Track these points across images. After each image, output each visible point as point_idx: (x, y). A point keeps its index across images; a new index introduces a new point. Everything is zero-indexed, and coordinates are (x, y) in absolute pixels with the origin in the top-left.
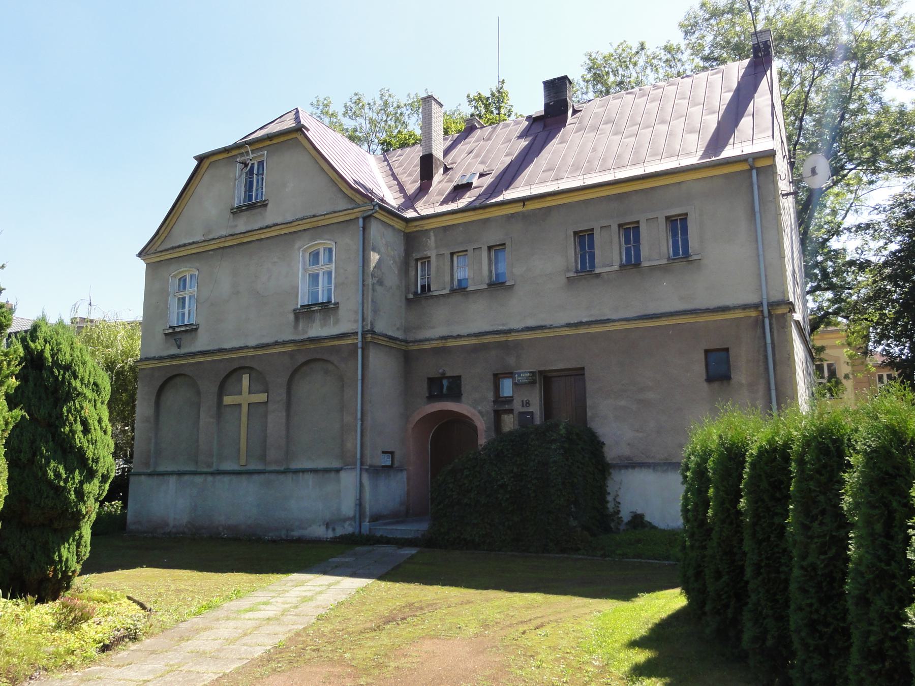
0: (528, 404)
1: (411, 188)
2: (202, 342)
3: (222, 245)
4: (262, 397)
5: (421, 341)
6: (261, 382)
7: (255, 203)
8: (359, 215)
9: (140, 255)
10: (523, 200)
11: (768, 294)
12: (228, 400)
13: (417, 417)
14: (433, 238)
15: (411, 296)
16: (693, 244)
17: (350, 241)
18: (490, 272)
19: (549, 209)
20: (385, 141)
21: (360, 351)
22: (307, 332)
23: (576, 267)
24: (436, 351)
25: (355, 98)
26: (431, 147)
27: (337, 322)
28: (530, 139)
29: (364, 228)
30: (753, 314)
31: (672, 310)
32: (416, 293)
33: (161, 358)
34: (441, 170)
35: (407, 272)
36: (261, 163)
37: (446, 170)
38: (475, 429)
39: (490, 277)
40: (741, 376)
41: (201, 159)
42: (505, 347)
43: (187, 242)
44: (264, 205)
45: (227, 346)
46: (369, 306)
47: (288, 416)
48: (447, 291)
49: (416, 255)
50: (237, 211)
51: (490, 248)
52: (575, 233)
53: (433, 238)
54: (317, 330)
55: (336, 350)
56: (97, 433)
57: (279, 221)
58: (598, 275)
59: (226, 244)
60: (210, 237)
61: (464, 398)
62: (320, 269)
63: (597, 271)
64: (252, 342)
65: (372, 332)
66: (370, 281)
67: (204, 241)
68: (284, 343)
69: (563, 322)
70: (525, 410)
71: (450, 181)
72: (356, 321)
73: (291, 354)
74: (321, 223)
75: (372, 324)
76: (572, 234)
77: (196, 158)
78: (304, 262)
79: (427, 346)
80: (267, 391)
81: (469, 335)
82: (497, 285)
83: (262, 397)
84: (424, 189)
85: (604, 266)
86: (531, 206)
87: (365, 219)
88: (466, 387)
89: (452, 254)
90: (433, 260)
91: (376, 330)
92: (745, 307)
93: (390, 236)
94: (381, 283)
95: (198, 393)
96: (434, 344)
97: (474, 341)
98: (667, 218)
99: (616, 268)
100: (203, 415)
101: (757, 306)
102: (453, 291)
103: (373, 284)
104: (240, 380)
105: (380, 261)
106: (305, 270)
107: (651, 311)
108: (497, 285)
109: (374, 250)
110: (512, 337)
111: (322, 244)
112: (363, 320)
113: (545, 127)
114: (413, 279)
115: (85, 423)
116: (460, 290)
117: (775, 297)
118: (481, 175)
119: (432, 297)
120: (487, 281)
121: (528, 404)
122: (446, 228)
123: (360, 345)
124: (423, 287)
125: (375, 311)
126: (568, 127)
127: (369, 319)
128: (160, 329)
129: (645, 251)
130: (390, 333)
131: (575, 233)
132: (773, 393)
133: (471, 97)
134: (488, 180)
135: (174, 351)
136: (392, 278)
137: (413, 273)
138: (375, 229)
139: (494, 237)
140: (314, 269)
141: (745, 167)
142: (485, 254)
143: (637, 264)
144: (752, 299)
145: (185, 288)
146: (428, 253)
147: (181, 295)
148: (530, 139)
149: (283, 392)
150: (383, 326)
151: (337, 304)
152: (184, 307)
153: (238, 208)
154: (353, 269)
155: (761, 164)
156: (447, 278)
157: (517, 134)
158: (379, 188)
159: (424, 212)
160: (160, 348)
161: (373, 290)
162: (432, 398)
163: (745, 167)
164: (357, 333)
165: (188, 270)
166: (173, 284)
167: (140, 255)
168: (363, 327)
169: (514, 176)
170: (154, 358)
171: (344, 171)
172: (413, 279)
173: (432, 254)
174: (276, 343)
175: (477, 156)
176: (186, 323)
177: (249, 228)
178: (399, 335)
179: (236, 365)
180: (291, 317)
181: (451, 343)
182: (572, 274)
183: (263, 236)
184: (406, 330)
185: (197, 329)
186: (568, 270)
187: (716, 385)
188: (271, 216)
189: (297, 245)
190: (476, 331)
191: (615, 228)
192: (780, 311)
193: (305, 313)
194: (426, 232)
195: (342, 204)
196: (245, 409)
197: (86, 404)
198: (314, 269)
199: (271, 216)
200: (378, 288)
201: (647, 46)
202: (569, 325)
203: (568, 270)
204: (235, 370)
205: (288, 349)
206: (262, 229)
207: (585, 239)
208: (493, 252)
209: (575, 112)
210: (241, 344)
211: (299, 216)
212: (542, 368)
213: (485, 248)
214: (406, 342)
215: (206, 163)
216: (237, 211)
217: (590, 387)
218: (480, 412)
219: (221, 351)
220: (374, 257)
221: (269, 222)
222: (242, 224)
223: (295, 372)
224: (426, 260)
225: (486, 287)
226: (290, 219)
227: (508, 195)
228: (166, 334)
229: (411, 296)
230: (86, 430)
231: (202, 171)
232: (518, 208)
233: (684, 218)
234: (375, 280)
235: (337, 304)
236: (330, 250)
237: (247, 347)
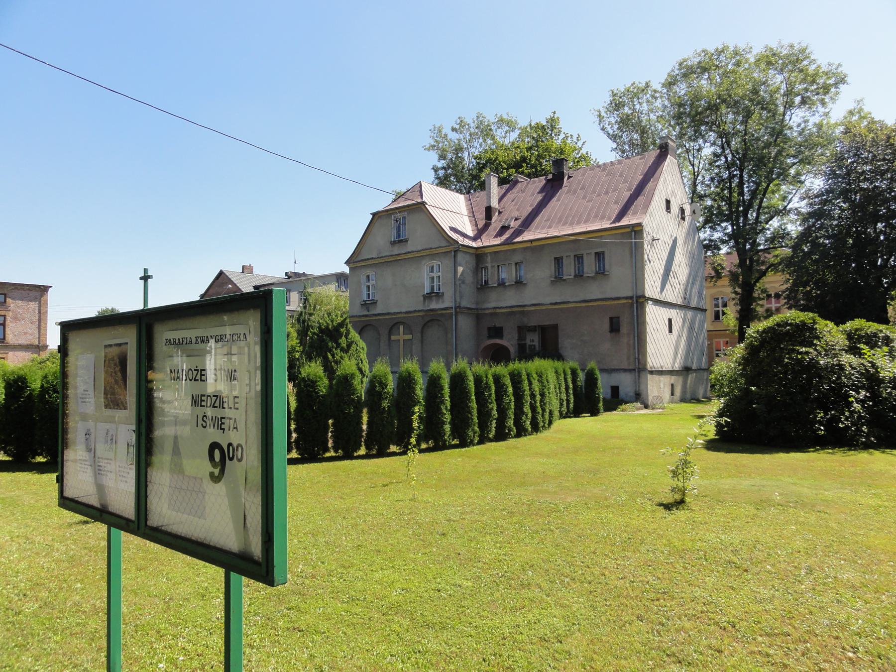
0: (533, 341)
1: (481, 224)
2: (379, 309)
3: (387, 260)
4: (410, 337)
5: (484, 309)
6: (409, 329)
7: (402, 240)
8: (452, 249)
9: (346, 263)
10: (531, 241)
11: (636, 292)
12: (393, 338)
13: (483, 346)
14: (489, 257)
15: (479, 287)
16: (607, 267)
17: (448, 262)
18: (516, 275)
19: (543, 245)
20: (477, 157)
21: (454, 317)
22: (429, 306)
23: (555, 275)
24: (492, 314)
25: (458, 122)
26: (490, 203)
27: (443, 302)
28: (544, 194)
29: (455, 256)
30: (630, 301)
31: (595, 298)
32: (481, 285)
33: (360, 316)
34: (497, 214)
35: (477, 274)
36: (404, 218)
37: (500, 213)
38: (509, 352)
39: (516, 277)
40: (624, 330)
41: (374, 215)
42: (523, 313)
43: (369, 257)
44: (406, 241)
45: (392, 311)
46: (458, 294)
47: (422, 337)
48: (496, 285)
49: (481, 266)
50: (393, 243)
51: (516, 264)
52: (555, 258)
53: (489, 257)
54: (434, 305)
55: (442, 315)
56: (365, 363)
57: (414, 250)
58: (565, 280)
59: (389, 260)
60: (381, 256)
61: (504, 337)
62: (435, 275)
63: (564, 278)
64: (404, 310)
65: (459, 307)
66: (458, 283)
67: (378, 258)
68: (419, 311)
69: (548, 302)
70: (532, 344)
71: (500, 221)
72: (452, 302)
73: (423, 317)
74: (434, 253)
75: (459, 303)
76: (553, 259)
77: (371, 214)
78: (427, 272)
79: (487, 312)
80: (411, 334)
81: (507, 307)
82: (519, 283)
83: (410, 337)
84: (487, 226)
85: (567, 276)
86: (534, 244)
87: (455, 251)
88: (505, 333)
89: (498, 266)
90: (490, 268)
91: (462, 306)
92: (627, 298)
93: (467, 257)
94: (463, 282)
95: (379, 334)
96: (490, 311)
97: (508, 310)
98: (596, 253)
99: (572, 277)
100: (382, 345)
101: (631, 298)
102: (499, 285)
103: (460, 284)
104: (399, 329)
105: (463, 271)
106: (427, 275)
107: (588, 298)
108: (519, 283)
109: (460, 266)
110: (526, 309)
111: (435, 263)
112: (455, 301)
113: (552, 187)
114: (480, 278)
115: (361, 360)
116: (502, 284)
117: (640, 294)
118: (516, 219)
119: (489, 287)
120: (514, 281)
121: (533, 341)
122: (496, 253)
123: (454, 313)
124: (485, 281)
125: (461, 297)
126: (563, 188)
127: (458, 300)
128: (358, 302)
129: (586, 269)
130: (469, 306)
131: (555, 258)
132: (636, 338)
133: (532, 125)
134: (519, 222)
135: (366, 313)
136: (469, 279)
137: (480, 275)
138: (460, 256)
139: (517, 258)
140: (432, 275)
141: (628, 230)
142: (513, 267)
143: (582, 276)
144: (629, 294)
145: (369, 280)
146: (487, 265)
147: (368, 284)
148: (544, 194)
149: (419, 335)
150: (464, 304)
151: (443, 293)
152: (369, 291)
153: (394, 241)
154: (450, 275)
155: (636, 229)
156: (496, 278)
157: (538, 191)
158: (463, 225)
159: (486, 244)
160: (358, 311)
161: (460, 286)
162: (490, 337)
163: (628, 230)
164: (452, 308)
165: (370, 272)
166: (364, 278)
167: (346, 263)
168: (455, 305)
169: (536, 213)
170: (356, 316)
171: (444, 223)
172: (480, 278)
173: (489, 265)
174: (415, 311)
175: (515, 205)
176: (371, 299)
177: (399, 252)
178: (473, 306)
179: (396, 321)
180: (422, 299)
181: (498, 311)
182: (553, 279)
183: (406, 257)
184: (477, 303)
185: (376, 302)
186: (551, 277)
187: (613, 334)
188: (410, 247)
189: (424, 262)
190: (510, 305)
191: (572, 257)
192: (641, 300)
193: (428, 297)
194: (486, 254)
195: (444, 243)
196: (402, 342)
197: (361, 354)
198: (432, 275)
199: (410, 247)
200: (462, 285)
201: (651, 84)
202: (551, 304)
203: (551, 277)
204: (398, 323)
205: (421, 314)
206: (406, 253)
207: (558, 261)
208: (518, 266)
209: (569, 177)
210: (397, 311)
211: (424, 248)
212: (540, 324)
213: (514, 264)
214: (477, 309)
215: (377, 216)
216: (393, 243)
217: (560, 333)
218: (512, 345)
219: (389, 314)
220: (460, 269)
221: (409, 250)
222: (396, 250)
223: (425, 325)
224: (486, 268)
225: (514, 283)
226: (420, 249)
227: (527, 236)
228: (362, 304)
229: (479, 287)
230: (362, 363)
231: (375, 221)
232: (529, 245)
233: (603, 253)
234: (460, 282)
235: (443, 293)
236: (439, 265)
237: (401, 313)
